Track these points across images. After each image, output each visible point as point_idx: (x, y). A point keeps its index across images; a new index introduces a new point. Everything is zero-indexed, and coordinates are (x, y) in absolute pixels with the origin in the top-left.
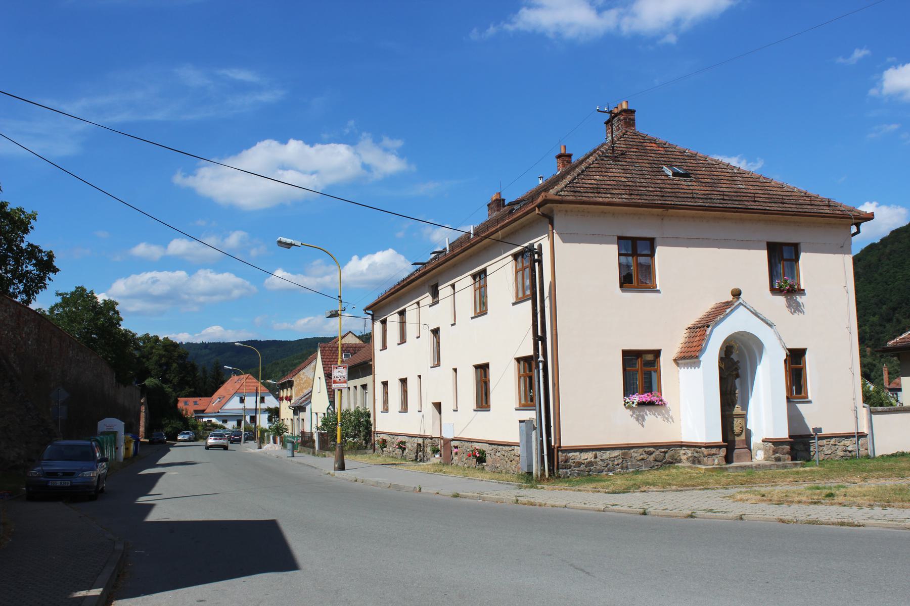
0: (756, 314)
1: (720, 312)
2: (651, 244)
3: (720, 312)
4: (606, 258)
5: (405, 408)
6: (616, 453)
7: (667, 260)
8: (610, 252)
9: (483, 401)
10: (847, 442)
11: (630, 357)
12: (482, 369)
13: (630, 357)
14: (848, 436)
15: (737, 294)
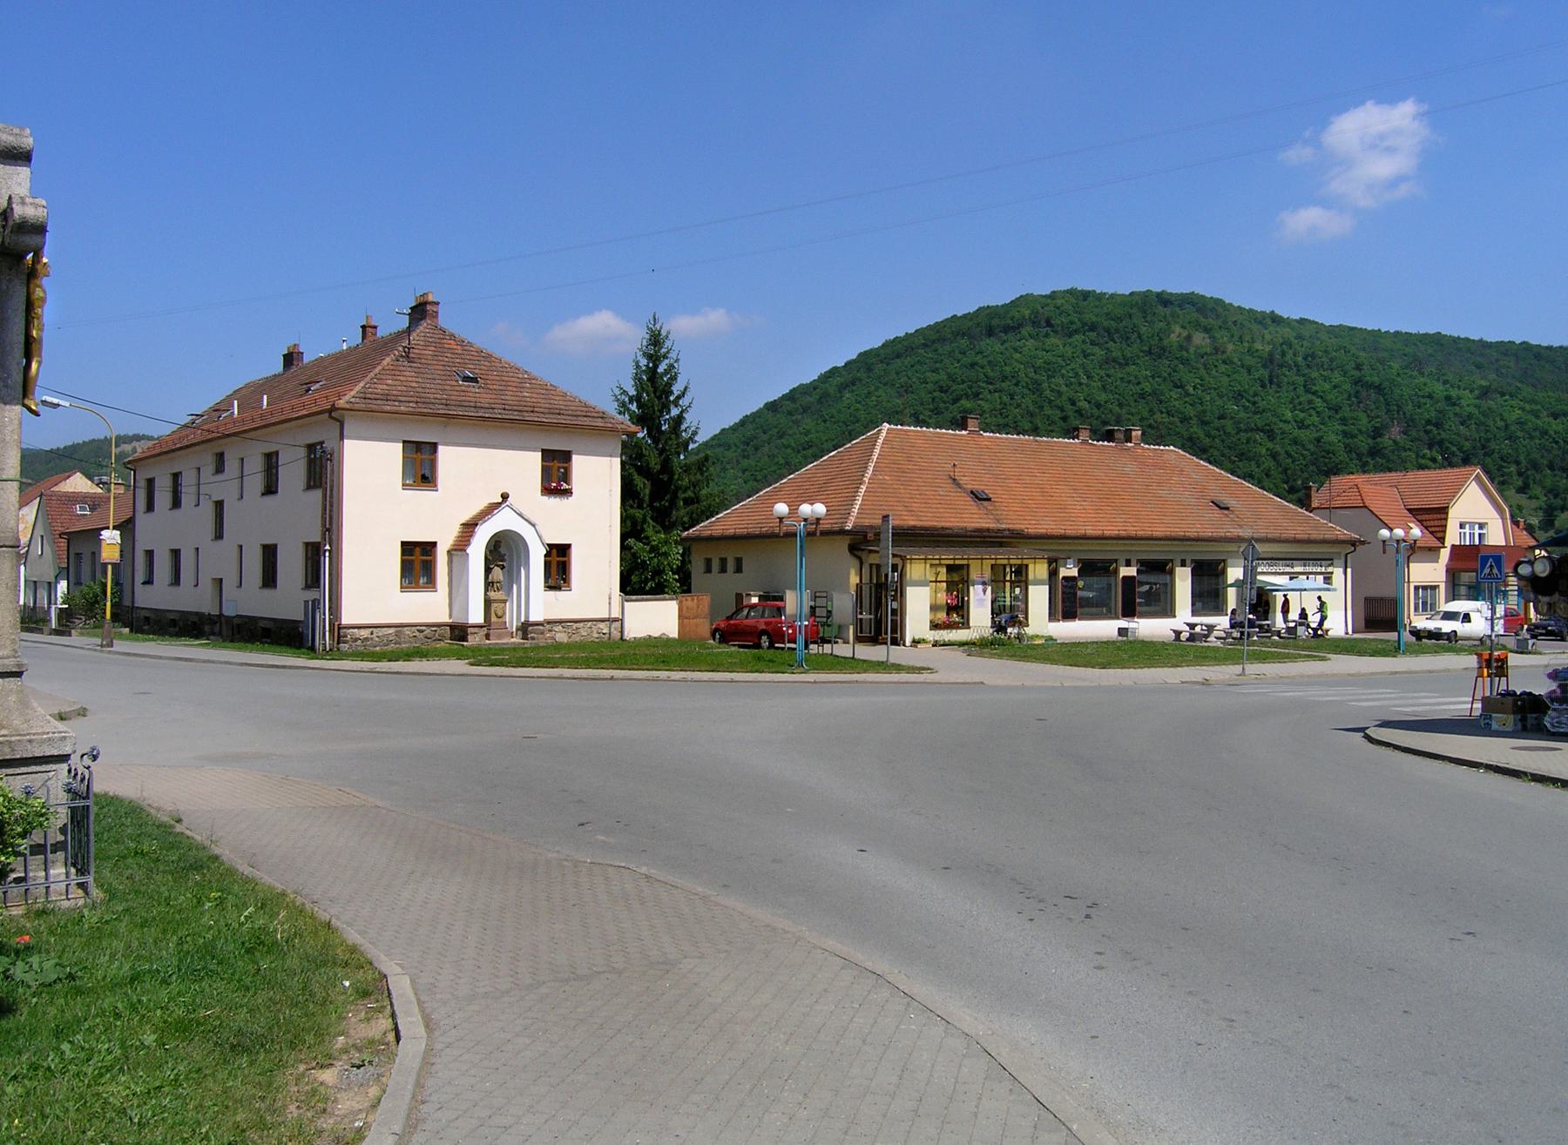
0: (520, 515)
1: (491, 509)
2: (566, 457)
3: (491, 509)
4: (393, 453)
5: (176, 580)
6: (391, 631)
7: (448, 457)
8: (395, 451)
9: (270, 578)
10: (602, 625)
11: (408, 548)
12: (176, 553)
13: (408, 548)
14: (602, 620)
15: (505, 497)
